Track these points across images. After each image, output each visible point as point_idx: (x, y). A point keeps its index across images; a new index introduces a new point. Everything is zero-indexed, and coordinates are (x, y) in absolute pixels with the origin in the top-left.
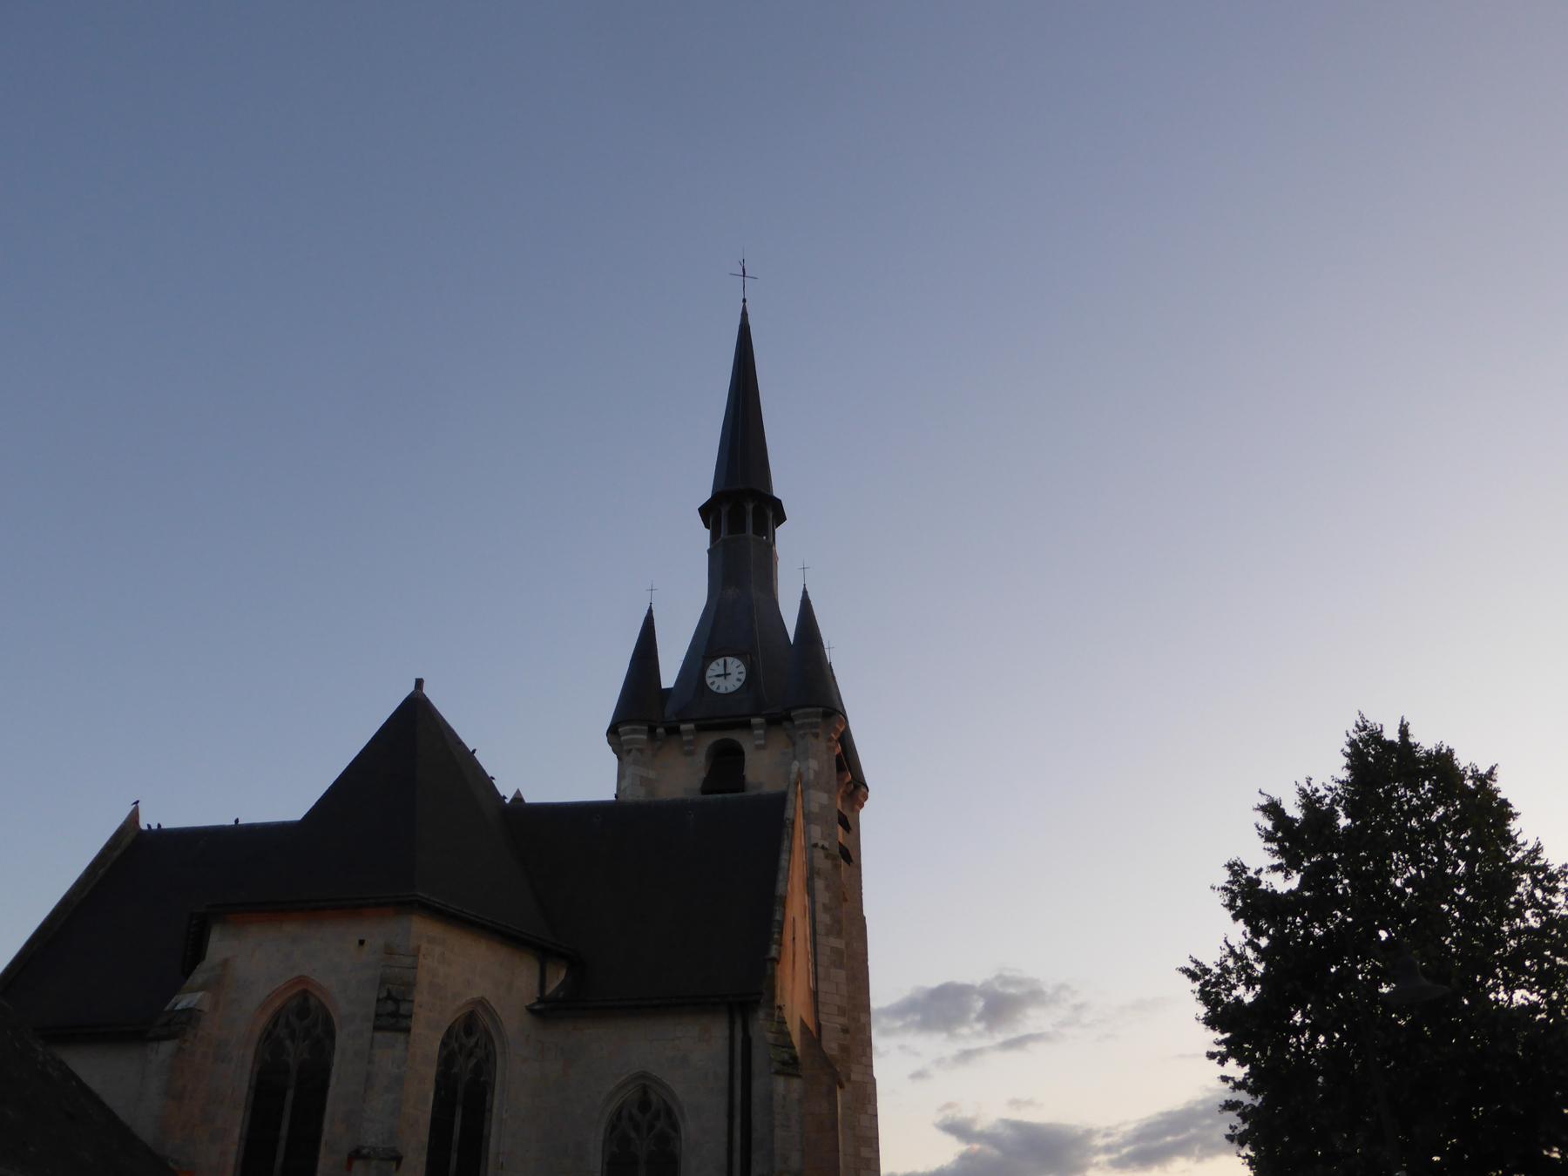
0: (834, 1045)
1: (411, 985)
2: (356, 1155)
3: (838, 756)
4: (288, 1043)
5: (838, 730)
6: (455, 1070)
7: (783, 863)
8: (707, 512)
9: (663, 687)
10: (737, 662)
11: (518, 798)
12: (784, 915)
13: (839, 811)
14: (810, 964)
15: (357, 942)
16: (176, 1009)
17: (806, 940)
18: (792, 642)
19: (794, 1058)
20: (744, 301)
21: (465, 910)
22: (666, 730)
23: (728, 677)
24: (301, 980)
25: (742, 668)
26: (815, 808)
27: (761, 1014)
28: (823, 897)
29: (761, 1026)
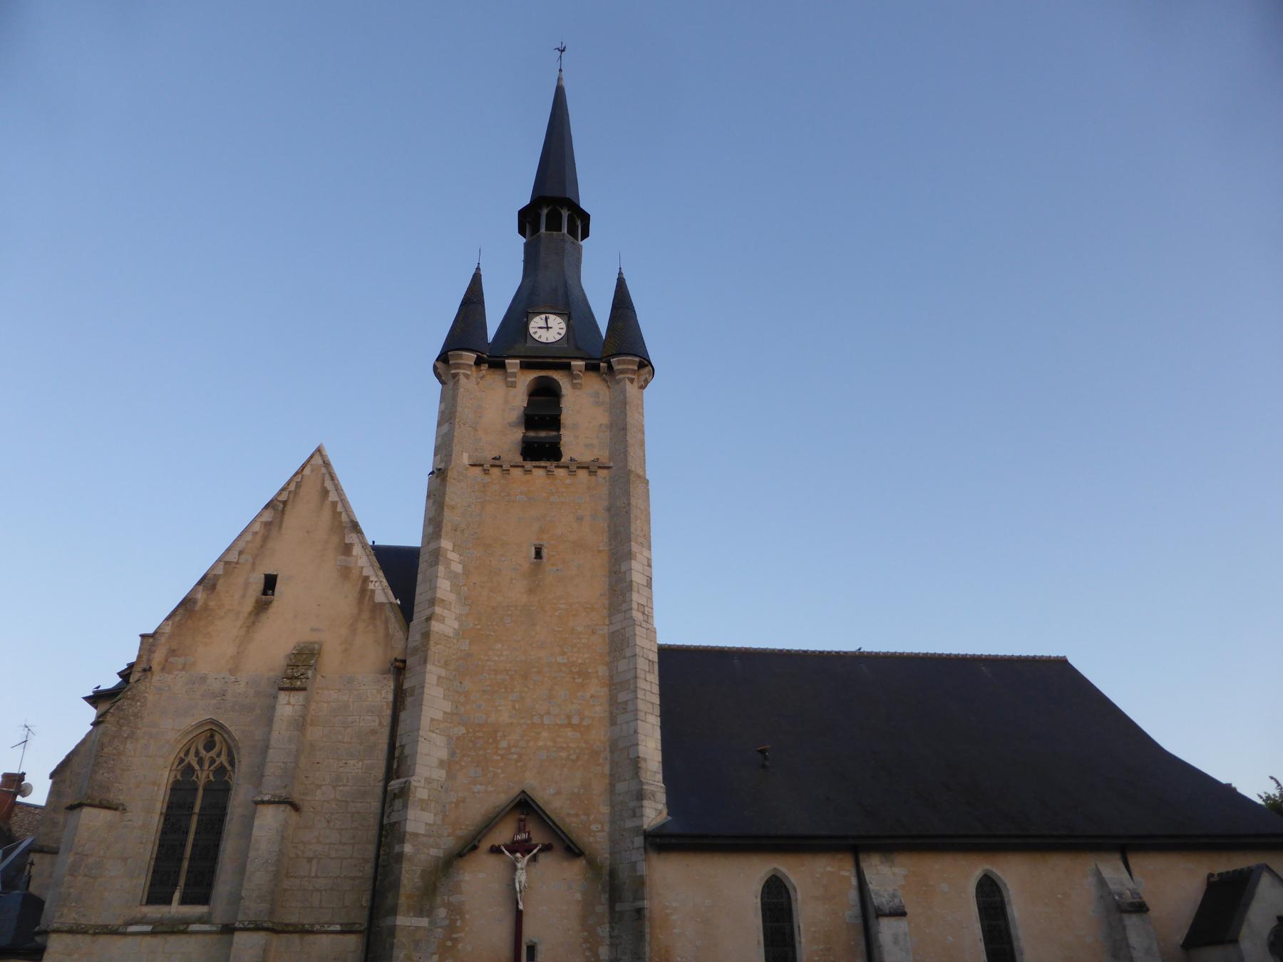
10: (559, 320)
18: (603, 329)
20: (560, 70)
25: (563, 325)
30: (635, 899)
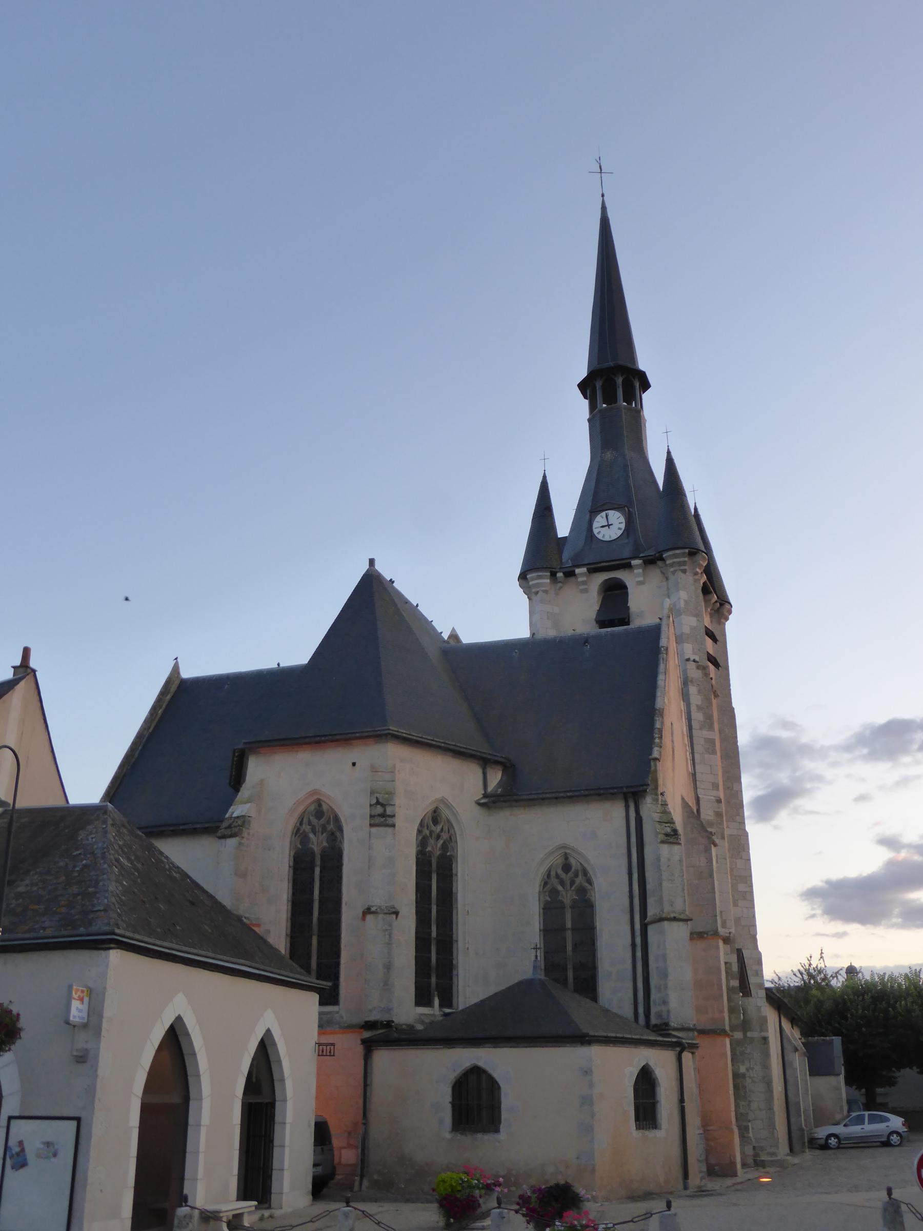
0: (711, 813)
1: (391, 794)
2: (368, 911)
3: (704, 583)
4: (311, 835)
5: (702, 565)
6: (429, 849)
7: (660, 683)
8: (585, 387)
9: (559, 536)
11: (454, 636)
12: (662, 723)
13: (706, 627)
14: (688, 753)
15: (351, 764)
16: (233, 816)
17: (683, 735)
19: (675, 832)
21: (424, 737)
22: (564, 573)
23: (610, 527)
24: (315, 792)
25: (622, 519)
26: (686, 630)
27: (649, 799)
28: (696, 699)
29: (649, 808)
30: (762, 1030)
